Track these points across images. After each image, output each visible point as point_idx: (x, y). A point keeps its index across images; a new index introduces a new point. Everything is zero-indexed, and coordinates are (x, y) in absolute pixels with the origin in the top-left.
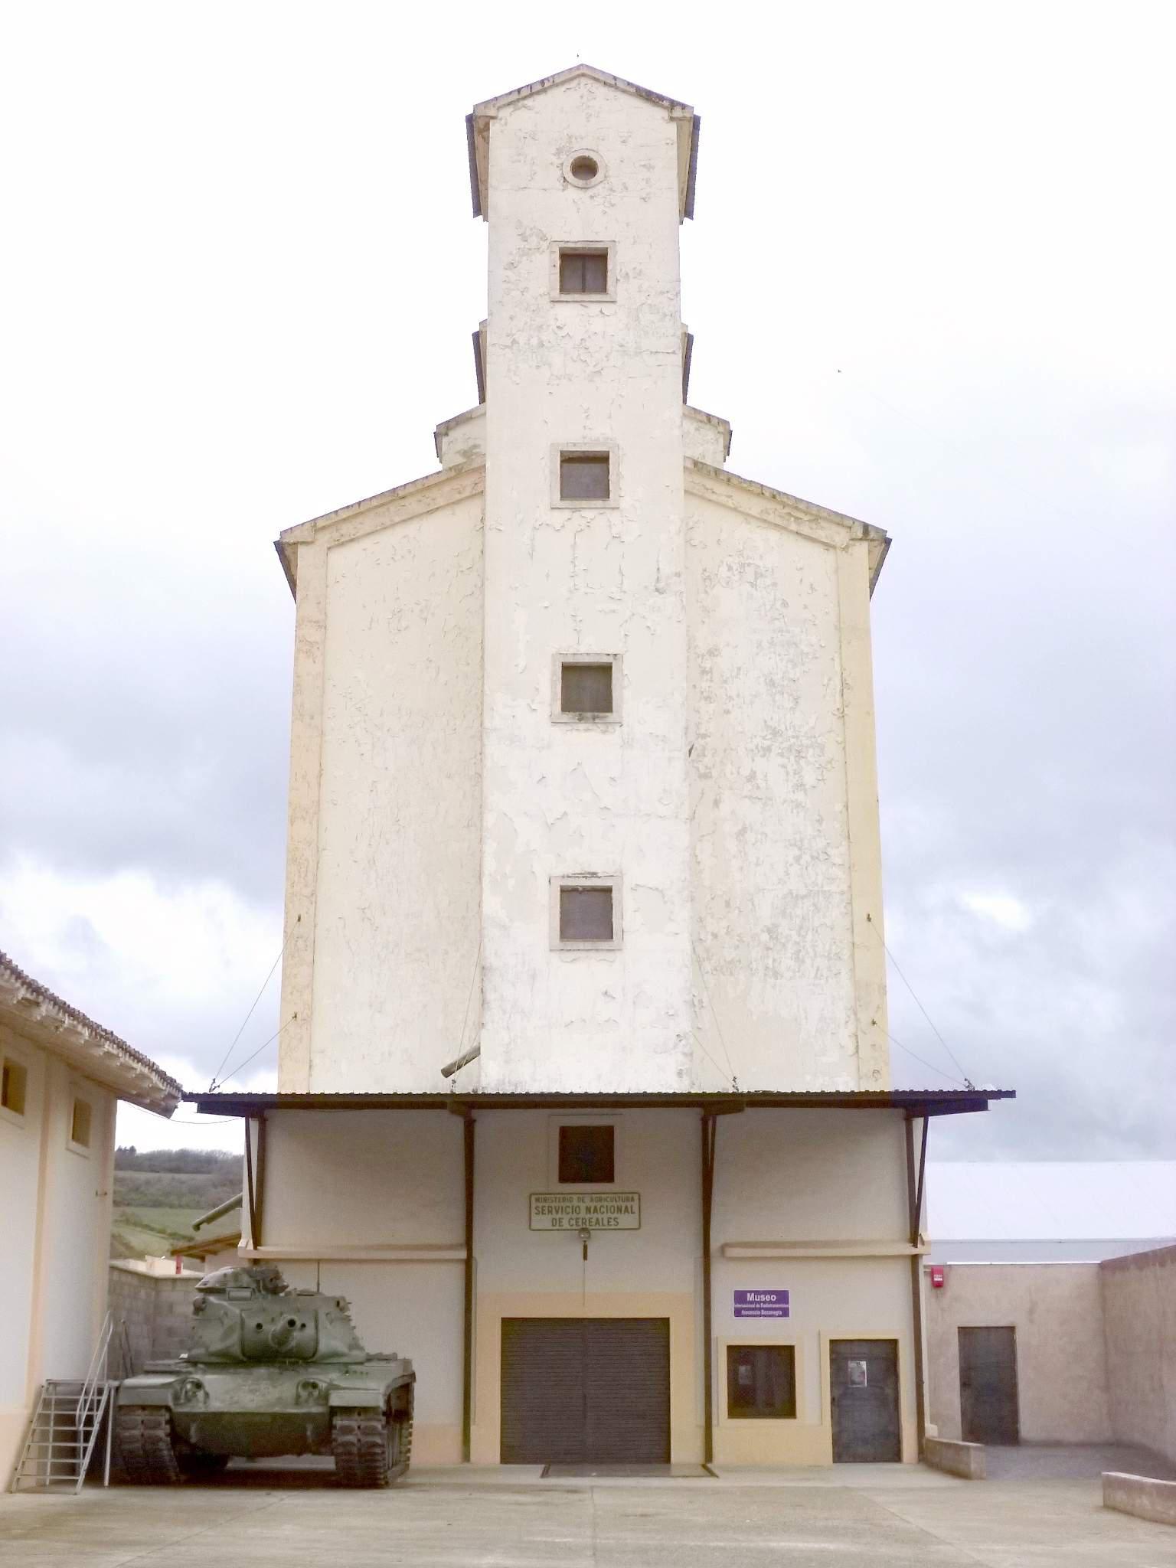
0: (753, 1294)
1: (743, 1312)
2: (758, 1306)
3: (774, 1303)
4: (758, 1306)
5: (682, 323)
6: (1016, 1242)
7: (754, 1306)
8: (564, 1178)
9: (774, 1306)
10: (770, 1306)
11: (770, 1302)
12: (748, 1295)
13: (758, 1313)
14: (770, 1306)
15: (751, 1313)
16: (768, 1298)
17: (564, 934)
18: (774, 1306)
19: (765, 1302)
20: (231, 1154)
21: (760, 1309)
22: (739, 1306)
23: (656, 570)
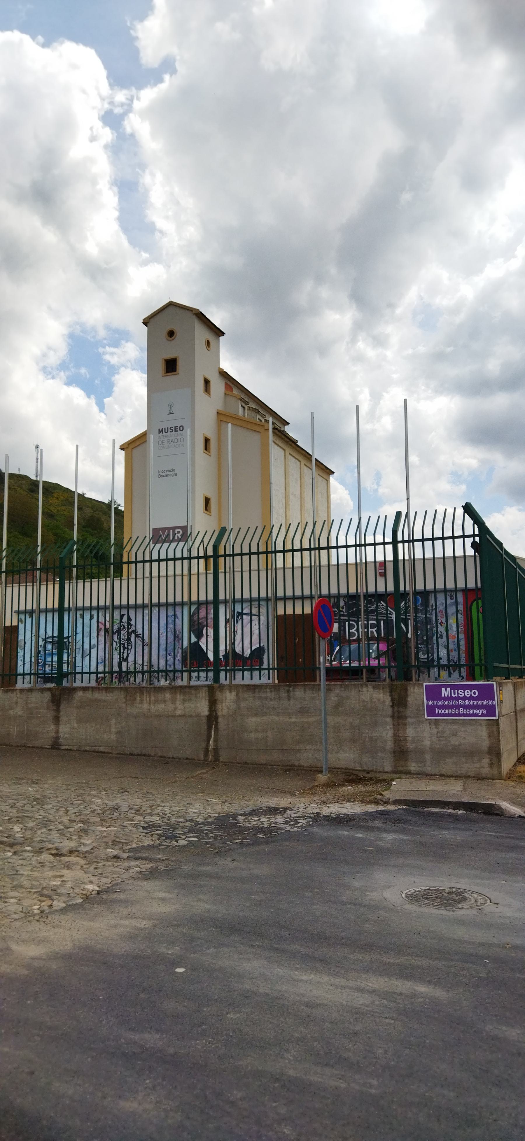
0: (449, 689)
1: (438, 711)
2: (455, 703)
3: (474, 699)
4: (455, 703)
5: (147, 326)
6: (327, 487)
7: (450, 703)
8: (154, 529)
9: (476, 703)
10: (471, 703)
11: (471, 698)
12: (443, 689)
13: (456, 711)
14: (471, 703)
15: (447, 711)
16: (467, 693)
17: (165, 360)
18: (476, 703)
19: (464, 698)
20: (74, 387)
21: (458, 707)
22: (432, 703)
23: (34, 447)
